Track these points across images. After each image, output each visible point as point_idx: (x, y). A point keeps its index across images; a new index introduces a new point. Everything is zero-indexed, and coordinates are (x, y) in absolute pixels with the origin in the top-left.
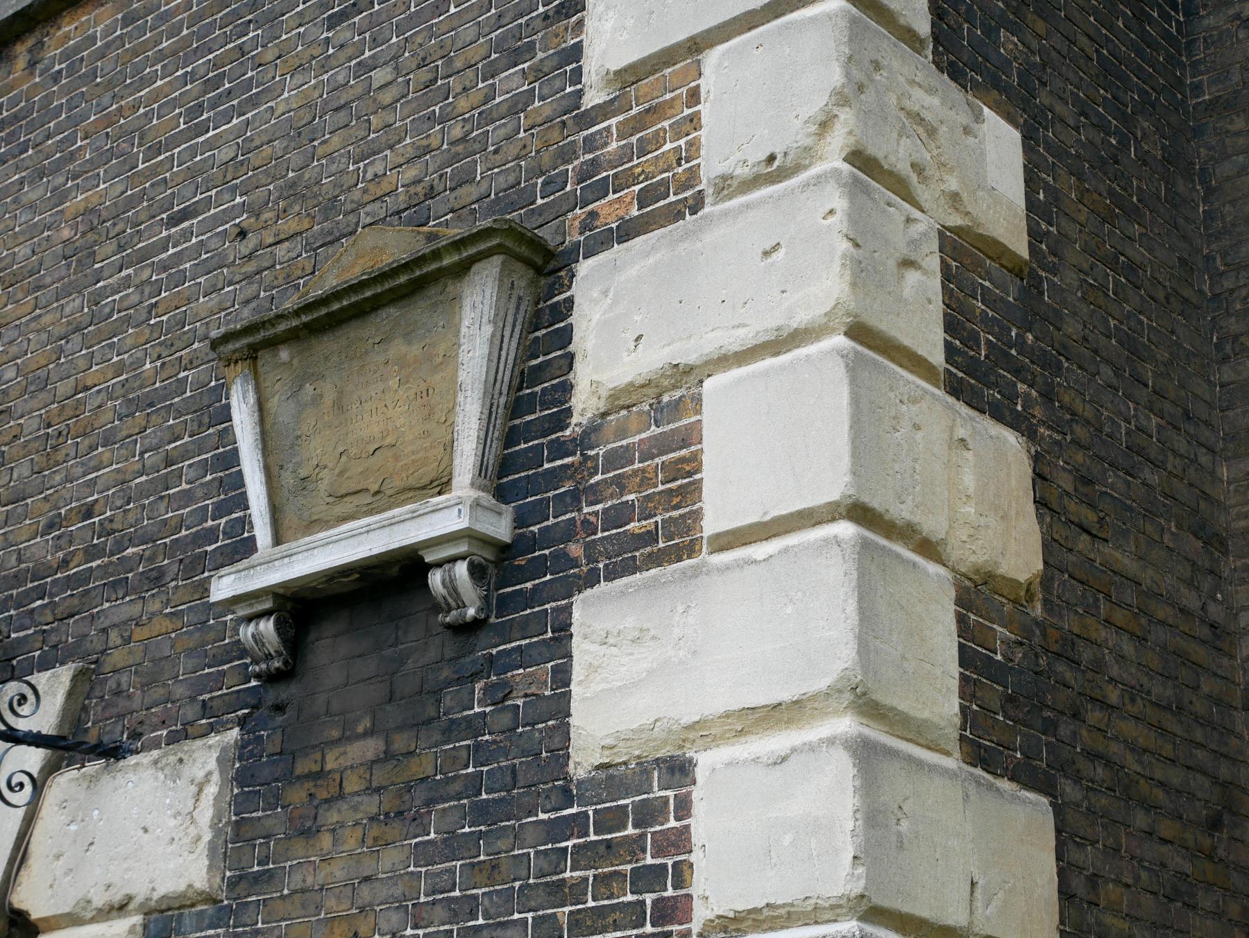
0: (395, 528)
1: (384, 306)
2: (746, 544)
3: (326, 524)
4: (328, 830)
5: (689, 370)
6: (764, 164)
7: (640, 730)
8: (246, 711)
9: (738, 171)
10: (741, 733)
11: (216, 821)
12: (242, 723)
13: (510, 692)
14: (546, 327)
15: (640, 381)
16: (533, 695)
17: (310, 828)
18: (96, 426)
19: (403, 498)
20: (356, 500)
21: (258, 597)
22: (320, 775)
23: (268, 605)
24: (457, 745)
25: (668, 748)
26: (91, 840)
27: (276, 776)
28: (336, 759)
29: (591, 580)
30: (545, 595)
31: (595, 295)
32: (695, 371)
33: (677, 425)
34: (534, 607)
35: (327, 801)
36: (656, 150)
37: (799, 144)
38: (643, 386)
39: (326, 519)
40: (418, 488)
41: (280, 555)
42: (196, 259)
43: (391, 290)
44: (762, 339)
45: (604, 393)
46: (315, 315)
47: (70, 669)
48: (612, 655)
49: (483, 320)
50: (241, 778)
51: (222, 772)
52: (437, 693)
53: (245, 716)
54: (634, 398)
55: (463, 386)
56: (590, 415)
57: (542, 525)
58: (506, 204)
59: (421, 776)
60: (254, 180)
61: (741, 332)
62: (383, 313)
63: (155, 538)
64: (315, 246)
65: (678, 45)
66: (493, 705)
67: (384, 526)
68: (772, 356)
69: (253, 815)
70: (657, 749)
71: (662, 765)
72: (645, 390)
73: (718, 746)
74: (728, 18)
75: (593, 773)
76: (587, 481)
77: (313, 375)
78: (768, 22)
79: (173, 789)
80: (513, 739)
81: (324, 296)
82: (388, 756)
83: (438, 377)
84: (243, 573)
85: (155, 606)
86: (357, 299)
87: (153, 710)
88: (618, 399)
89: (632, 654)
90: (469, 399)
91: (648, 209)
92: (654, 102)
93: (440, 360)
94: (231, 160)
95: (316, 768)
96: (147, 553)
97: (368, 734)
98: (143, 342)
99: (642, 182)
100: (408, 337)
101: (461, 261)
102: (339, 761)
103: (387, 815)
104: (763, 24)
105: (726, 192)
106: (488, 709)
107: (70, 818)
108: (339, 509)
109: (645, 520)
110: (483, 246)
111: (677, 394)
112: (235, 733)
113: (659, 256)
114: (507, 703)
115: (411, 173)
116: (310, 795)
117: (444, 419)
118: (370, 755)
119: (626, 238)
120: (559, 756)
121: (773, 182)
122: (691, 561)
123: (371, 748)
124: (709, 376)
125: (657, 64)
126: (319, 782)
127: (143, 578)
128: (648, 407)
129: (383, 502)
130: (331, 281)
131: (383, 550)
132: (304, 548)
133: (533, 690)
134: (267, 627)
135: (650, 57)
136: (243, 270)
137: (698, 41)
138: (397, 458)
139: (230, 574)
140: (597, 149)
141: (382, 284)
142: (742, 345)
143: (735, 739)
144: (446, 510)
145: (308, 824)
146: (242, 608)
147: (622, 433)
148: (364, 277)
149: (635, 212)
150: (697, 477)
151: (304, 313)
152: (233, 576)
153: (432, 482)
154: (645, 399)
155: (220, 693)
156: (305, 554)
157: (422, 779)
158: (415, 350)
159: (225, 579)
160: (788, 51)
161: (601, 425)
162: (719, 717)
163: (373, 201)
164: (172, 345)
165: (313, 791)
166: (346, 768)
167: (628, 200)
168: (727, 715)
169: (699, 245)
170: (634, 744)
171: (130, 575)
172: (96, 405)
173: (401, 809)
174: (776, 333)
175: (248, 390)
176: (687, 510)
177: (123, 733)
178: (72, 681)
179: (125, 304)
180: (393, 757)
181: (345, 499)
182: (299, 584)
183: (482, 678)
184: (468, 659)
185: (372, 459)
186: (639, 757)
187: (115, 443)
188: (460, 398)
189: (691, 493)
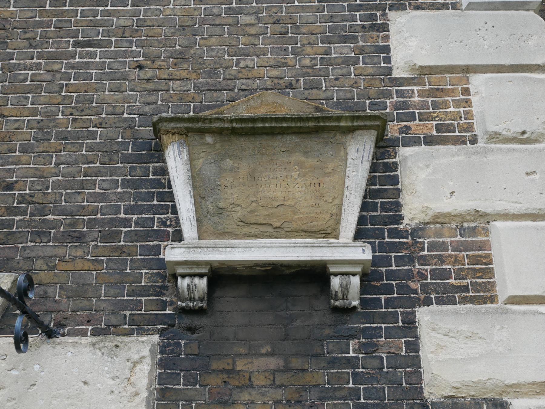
0: (315, 249)
1: (288, 134)
2: (527, 304)
3: (236, 236)
4: (242, 404)
5: (486, 214)
6: (520, 134)
7: (479, 382)
8: (165, 327)
9: (504, 133)
10: (537, 393)
11: (149, 387)
12: (161, 333)
13: (377, 349)
14: (380, 172)
15: (455, 213)
16: (394, 353)
17: (227, 401)
18: (12, 139)
19: (296, 234)
20: (262, 228)
21: (199, 265)
22: (232, 372)
23: (204, 271)
24: (339, 371)
25: (492, 394)
26: (33, 383)
27: (195, 367)
28: (245, 365)
29: (428, 302)
30: (396, 304)
31: (421, 166)
32: (487, 217)
33: (474, 239)
34: (388, 309)
35: (238, 387)
36: (445, 109)
37: (539, 131)
38: (455, 216)
39: (236, 233)
40: (309, 232)
41: (224, 246)
42: (101, 70)
43: (301, 127)
44: (531, 212)
45: (431, 213)
46: (243, 126)
47: (11, 276)
48: (453, 342)
49: (364, 159)
50: (163, 364)
51: (153, 358)
52: (321, 340)
53: (163, 329)
54: (447, 220)
55: (349, 188)
56: (417, 221)
57: (388, 268)
58: (345, 106)
59: (314, 384)
60: (300, 50)
61: (518, 206)
62: (288, 138)
63: (74, 214)
64: (203, 89)
65: (459, 66)
66: (365, 354)
67: (307, 247)
68: (531, 221)
69: (175, 387)
70: (485, 393)
71: (489, 402)
72: (455, 218)
73: (522, 398)
74: (489, 63)
75: (442, 400)
76: (418, 253)
77: (232, 155)
78: (508, 72)
79: (111, 362)
80: (382, 374)
81: (256, 118)
82: (287, 369)
83: (327, 179)
84: (192, 250)
85: (80, 253)
86: (276, 125)
87: (78, 313)
88: (438, 218)
89: (467, 344)
90: (353, 196)
91: (443, 134)
92: (441, 87)
93: (330, 170)
94: (128, 26)
95: (230, 367)
96: (68, 221)
97: (268, 354)
98: (57, 103)
99: (437, 121)
100: (305, 153)
101: (353, 126)
102: (247, 366)
103: (288, 401)
104: (505, 73)
105: (494, 140)
106: (361, 356)
107: (12, 366)
108: (247, 230)
109: (460, 279)
110: (368, 123)
111: (473, 225)
112: (156, 338)
113: (460, 158)
114: (374, 354)
115: (275, 73)
116: (225, 382)
117: (331, 201)
118: (272, 366)
119: (430, 144)
120: (417, 388)
121: (521, 143)
122: (492, 305)
123: (274, 363)
124: (494, 221)
125: (443, 70)
126: (231, 376)
127: (65, 235)
128: (454, 226)
129: (281, 233)
130: (243, 111)
131: (309, 259)
132: (244, 245)
133: (392, 350)
134: (202, 284)
135: (441, 66)
136: (143, 86)
137: (470, 68)
138: (294, 213)
139: (181, 248)
140: (406, 98)
141: (296, 123)
142: (518, 211)
143: (533, 396)
144: (353, 248)
145: (226, 398)
146: (183, 268)
147: (439, 234)
148: (287, 116)
149: (434, 133)
150: (491, 266)
151: (236, 123)
152: (183, 250)
153: (320, 231)
154: (453, 222)
155: (139, 312)
156: (245, 249)
157: (314, 385)
158: (311, 162)
159: (176, 250)
160: (528, 89)
161: (425, 228)
162: (529, 384)
163: (246, 78)
164: (82, 111)
165: (227, 380)
166: (253, 371)
167: (430, 126)
168: (534, 384)
169: (485, 159)
170: (472, 388)
171: (53, 231)
172: (13, 127)
173: (300, 399)
174: (538, 211)
175: (183, 151)
176: (486, 280)
177: (51, 322)
178: (12, 283)
179: (38, 78)
180: (290, 370)
181: (252, 226)
182: (231, 264)
183: (356, 338)
184: (343, 327)
185: (275, 210)
186: (473, 396)
187: (33, 153)
188: (346, 193)
189: (488, 273)
